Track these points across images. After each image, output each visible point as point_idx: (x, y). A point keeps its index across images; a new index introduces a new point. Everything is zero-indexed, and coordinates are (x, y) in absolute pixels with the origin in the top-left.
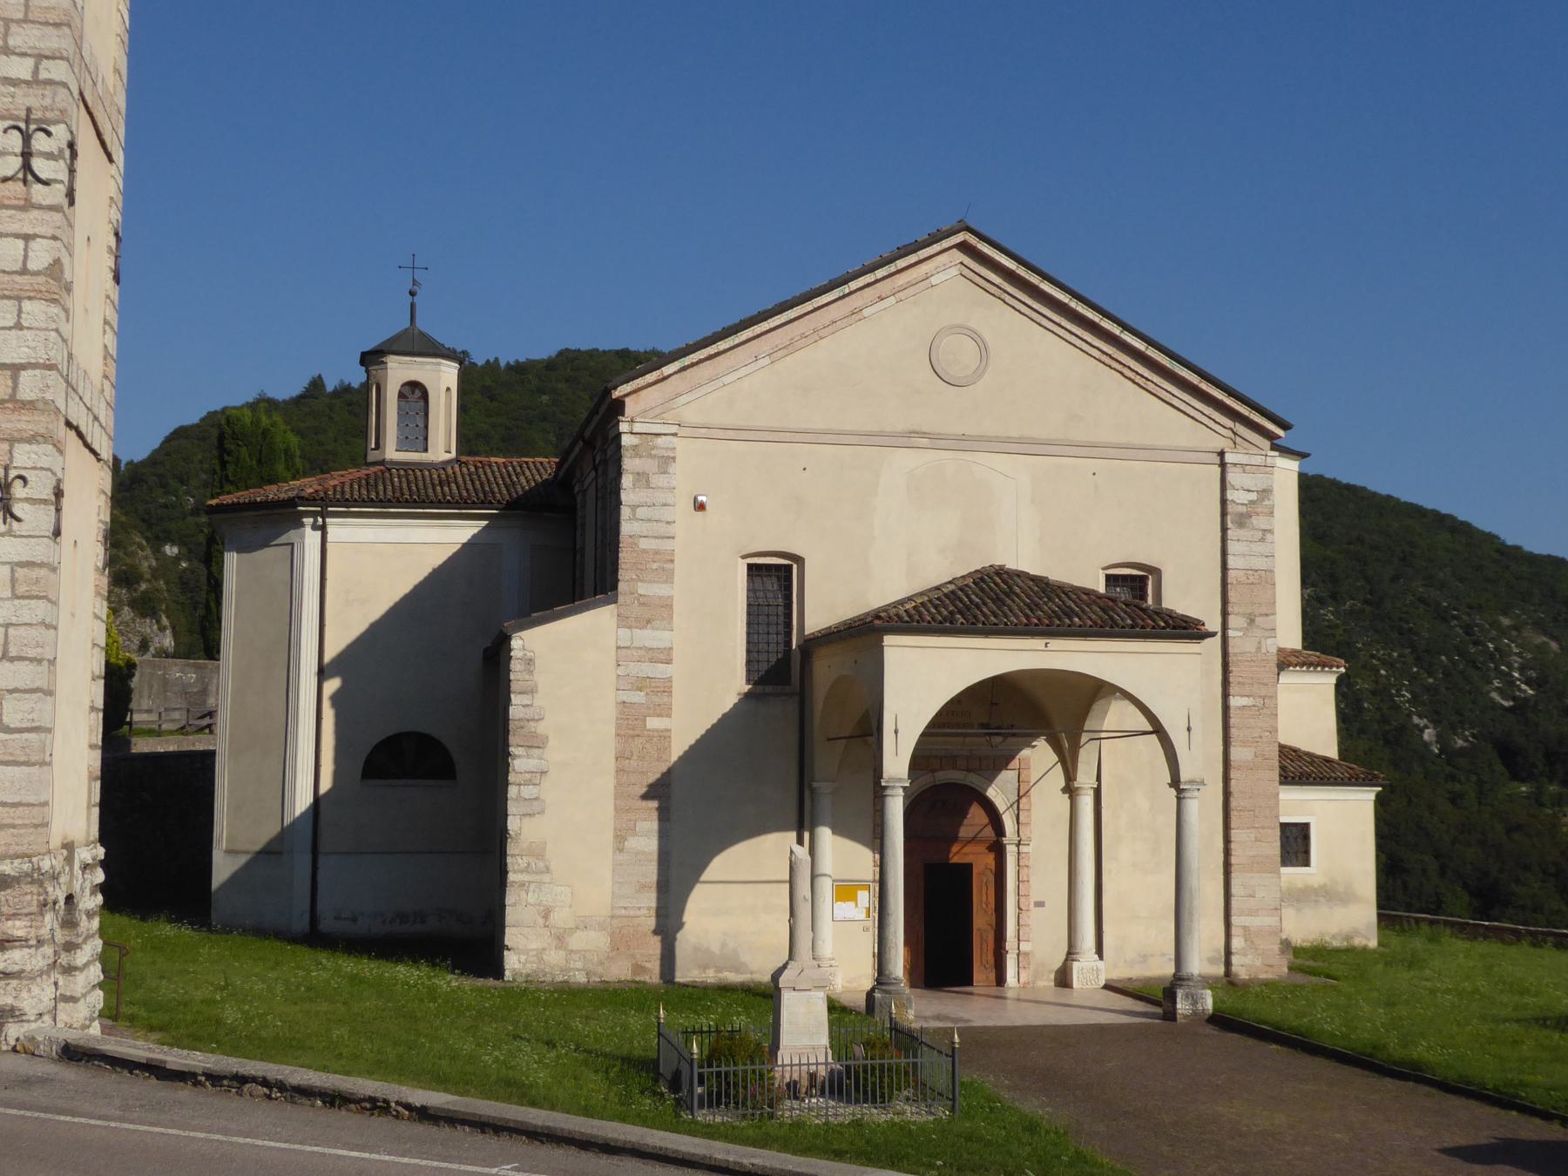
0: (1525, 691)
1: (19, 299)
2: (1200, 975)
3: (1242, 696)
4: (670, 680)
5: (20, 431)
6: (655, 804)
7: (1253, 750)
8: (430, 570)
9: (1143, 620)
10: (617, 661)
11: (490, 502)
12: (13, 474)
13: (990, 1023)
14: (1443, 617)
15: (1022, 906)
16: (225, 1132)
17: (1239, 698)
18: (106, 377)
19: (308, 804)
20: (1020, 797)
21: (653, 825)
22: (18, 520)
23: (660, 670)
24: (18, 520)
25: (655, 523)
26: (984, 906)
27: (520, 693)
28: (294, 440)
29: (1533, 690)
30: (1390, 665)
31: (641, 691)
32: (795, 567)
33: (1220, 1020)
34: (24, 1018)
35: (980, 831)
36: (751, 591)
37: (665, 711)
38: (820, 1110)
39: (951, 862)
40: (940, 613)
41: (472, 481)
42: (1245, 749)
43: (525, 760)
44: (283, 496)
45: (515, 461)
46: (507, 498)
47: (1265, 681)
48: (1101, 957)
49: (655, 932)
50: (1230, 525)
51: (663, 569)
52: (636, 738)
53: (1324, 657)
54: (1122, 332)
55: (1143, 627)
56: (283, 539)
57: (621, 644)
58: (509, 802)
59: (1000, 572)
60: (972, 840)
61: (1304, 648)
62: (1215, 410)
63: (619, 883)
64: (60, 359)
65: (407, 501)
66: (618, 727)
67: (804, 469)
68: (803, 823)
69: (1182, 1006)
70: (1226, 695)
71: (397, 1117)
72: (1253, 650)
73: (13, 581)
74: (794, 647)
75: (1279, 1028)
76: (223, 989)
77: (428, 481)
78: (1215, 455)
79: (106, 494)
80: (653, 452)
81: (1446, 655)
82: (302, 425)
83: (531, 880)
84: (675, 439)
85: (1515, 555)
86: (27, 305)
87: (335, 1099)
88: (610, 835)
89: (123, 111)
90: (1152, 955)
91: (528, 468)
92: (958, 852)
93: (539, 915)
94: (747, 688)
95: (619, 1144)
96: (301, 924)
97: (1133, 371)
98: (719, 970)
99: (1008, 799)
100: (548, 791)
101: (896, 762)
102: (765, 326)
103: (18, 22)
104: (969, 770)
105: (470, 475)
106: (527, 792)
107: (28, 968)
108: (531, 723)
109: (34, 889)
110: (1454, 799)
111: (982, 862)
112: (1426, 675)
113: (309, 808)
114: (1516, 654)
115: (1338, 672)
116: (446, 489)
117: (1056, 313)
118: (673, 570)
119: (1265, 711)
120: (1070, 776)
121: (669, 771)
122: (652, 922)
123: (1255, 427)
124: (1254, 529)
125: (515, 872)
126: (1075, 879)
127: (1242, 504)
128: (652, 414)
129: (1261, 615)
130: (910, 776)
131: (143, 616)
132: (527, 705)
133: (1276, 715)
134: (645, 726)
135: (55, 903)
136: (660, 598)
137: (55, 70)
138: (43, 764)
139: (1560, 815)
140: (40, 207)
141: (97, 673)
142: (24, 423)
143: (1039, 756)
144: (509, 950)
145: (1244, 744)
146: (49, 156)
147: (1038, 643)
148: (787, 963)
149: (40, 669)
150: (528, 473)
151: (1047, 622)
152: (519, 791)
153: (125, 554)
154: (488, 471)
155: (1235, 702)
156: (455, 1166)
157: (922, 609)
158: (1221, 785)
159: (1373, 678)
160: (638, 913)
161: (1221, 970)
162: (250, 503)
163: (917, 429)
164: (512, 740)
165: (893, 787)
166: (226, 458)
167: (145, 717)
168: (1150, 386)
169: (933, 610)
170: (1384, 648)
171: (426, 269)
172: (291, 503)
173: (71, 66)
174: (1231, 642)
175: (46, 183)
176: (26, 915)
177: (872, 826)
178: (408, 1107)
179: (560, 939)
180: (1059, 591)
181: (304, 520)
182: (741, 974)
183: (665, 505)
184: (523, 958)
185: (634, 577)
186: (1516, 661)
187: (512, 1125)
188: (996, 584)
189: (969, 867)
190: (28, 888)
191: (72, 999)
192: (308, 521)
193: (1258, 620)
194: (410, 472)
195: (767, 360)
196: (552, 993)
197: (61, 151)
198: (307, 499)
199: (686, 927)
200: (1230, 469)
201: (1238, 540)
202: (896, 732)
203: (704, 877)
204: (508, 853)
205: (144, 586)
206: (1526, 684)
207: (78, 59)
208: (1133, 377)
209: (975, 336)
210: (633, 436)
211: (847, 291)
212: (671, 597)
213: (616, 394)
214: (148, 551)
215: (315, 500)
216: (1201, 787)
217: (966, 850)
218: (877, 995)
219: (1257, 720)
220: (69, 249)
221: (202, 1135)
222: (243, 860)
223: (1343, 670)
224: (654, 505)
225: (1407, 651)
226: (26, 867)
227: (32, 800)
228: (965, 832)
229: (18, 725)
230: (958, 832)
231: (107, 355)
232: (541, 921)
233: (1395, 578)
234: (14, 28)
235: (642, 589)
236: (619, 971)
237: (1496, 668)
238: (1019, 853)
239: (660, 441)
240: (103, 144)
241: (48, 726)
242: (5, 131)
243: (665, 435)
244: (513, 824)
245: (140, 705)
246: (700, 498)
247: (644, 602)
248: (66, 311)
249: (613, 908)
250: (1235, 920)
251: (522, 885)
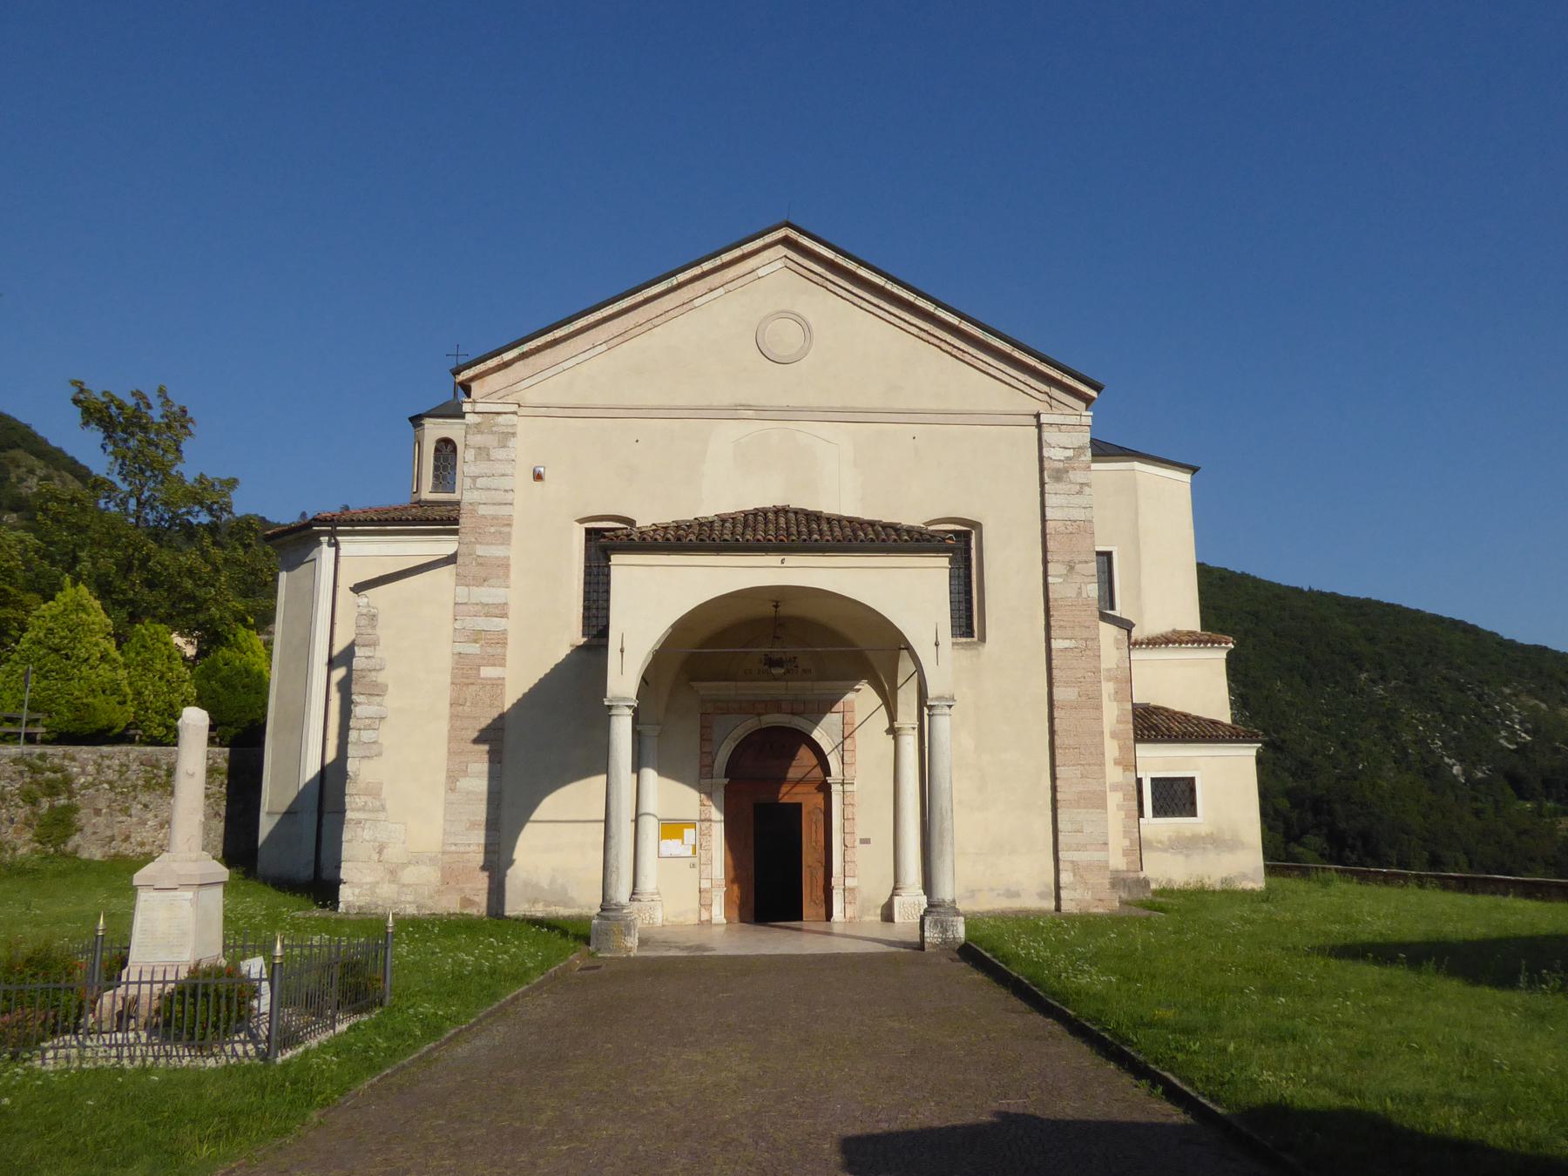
0: (1524, 738)
3: (1063, 639)
4: (505, 632)
7: (1076, 690)
10: (455, 616)
14: (1461, 689)
15: (847, 844)
17: (1061, 640)
19: (316, 772)
23: (496, 624)
25: (493, 492)
26: (814, 844)
27: (363, 646)
29: (1530, 736)
30: (1426, 723)
31: (476, 643)
35: (809, 772)
37: (500, 661)
39: (781, 801)
42: (1069, 689)
47: (1086, 624)
49: (483, 868)
52: (470, 686)
53: (1214, 636)
54: (936, 309)
56: (310, 557)
57: (458, 600)
58: (349, 746)
60: (798, 782)
62: (1031, 377)
63: (451, 821)
66: (454, 676)
67: (637, 441)
78: (1032, 417)
80: (494, 429)
81: (1465, 715)
83: (366, 817)
84: (514, 417)
85: (1511, 645)
88: (442, 776)
90: (980, 890)
92: (787, 793)
93: (374, 850)
94: (581, 641)
97: (949, 344)
98: (547, 904)
99: (833, 741)
100: (386, 735)
104: (793, 714)
108: (374, 673)
110: (1477, 813)
111: (810, 801)
112: (1451, 729)
114: (1516, 713)
115: (1225, 648)
117: (874, 296)
118: (509, 534)
119: (1088, 652)
120: (892, 717)
122: (480, 859)
123: (1057, 385)
124: (1071, 482)
125: (353, 810)
127: (1060, 461)
129: (1080, 562)
132: (370, 657)
133: (1099, 656)
134: (479, 675)
136: (497, 558)
139: (1557, 823)
144: (345, 883)
145: (1067, 684)
147: (773, 560)
152: (359, 735)
155: (1055, 644)
158: (1047, 724)
159: (1414, 732)
160: (468, 849)
161: (1052, 905)
163: (744, 402)
165: (618, 707)
168: (967, 358)
170: (1420, 712)
171: (458, 346)
174: (1051, 588)
177: (698, 767)
181: (321, 538)
182: (569, 908)
183: (503, 475)
184: (357, 891)
185: (473, 540)
186: (1517, 718)
189: (798, 807)
192: (324, 539)
193: (1078, 567)
198: (320, 520)
199: (516, 863)
200: (1045, 428)
201: (1056, 494)
202: (622, 651)
203: (534, 817)
204: (347, 792)
206: (1525, 733)
208: (950, 350)
209: (799, 320)
210: (476, 415)
217: (795, 790)
219: (1080, 661)
222: (277, 818)
223: (1231, 646)
224: (493, 475)
225: (1437, 714)
228: (793, 773)
230: (787, 772)
232: (376, 857)
233: (1426, 664)
236: (449, 904)
237: (1503, 723)
239: (501, 419)
243: (505, 413)
247: (482, 562)
251: (359, 822)
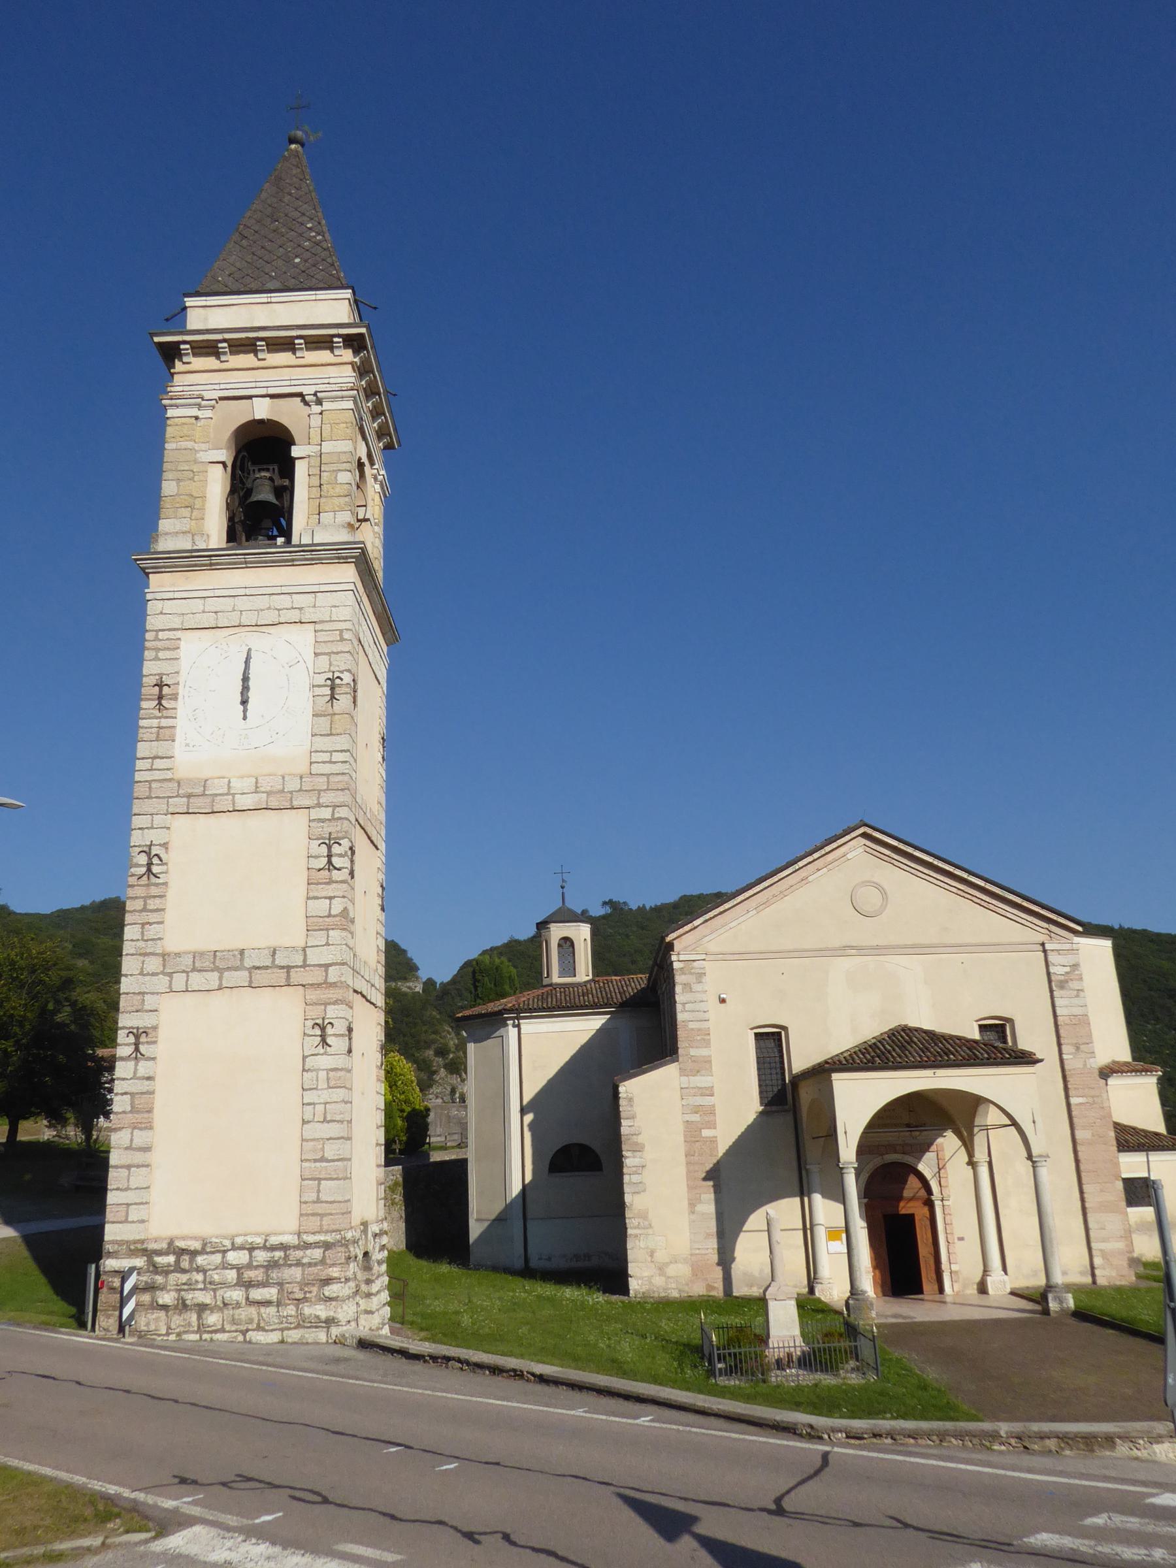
1: (327, 930)
2: (1063, 1284)
3: (1078, 1097)
4: (714, 1106)
5: (329, 998)
6: (711, 1183)
8: (579, 1046)
9: (995, 1054)
11: (611, 1004)
12: (326, 1021)
13: (927, 1319)
16: (433, 1390)
18: (379, 962)
20: (940, 1169)
21: (711, 1196)
22: (330, 1046)
23: (707, 1101)
24: (330, 1046)
28: (514, 971)
32: (783, 1033)
33: (1080, 1315)
34: (340, 1323)
36: (758, 1049)
37: (712, 1125)
38: (795, 1376)
40: (865, 1057)
41: (601, 992)
43: (631, 1159)
44: (496, 1009)
45: (626, 978)
46: (620, 1000)
47: (1093, 1086)
48: (1006, 1273)
49: (718, 1264)
50: (1054, 988)
51: (704, 1040)
53: (1146, 1066)
55: (995, 1059)
56: (497, 1034)
57: (683, 1086)
59: (905, 1029)
61: (1134, 1059)
64: (348, 959)
65: (563, 1007)
66: (685, 1136)
68: (803, 1191)
69: (1053, 1305)
70: (1067, 1097)
71: (527, 1381)
72: (1082, 1067)
73: (328, 1079)
74: (787, 1082)
75: (1114, 1319)
76: (465, 1304)
77: (576, 993)
79: (381, 1025)
80: (693, 971)
82: (535, 953)
86: (331, 932)
87: (496, 1370)
88: (686, 1203)
89: (384, 822)
91: (634, 982)
94: (761, 1108)
95: (645, 1397)
96: (519, 1264)
101: (848, 1152)
102: (751, 892)
103: (324, 790)
105: (600, 988)
106: (635, 1178)
107: (341, 1295)
108: (634, 1137)
109: (343, 1249)
111: (921, 1212)
113: (519, 1194)
116: (586, 998)
118: (710, 1040)
121: (718, 1162)
122: (715, 1258)
125: (631, 1228)
126: (984, 1221)
128: (690, 949)
129: (1083, 1044)
130: (857, 1161)
131: (452, 1073)
135: (356, 1257)
136: (704, 1057)
137: (342, 812)
138: (345, 1178)
140: (337, 882)
141: (379, 1124)
142: (332, 994)
143: (949, 1142)
146: (340, 855)
147: (928, 1072)
148: (770, 1283)
149: (342, 1126)
150: (633, 984)
151: (933, 1059)
153: (441, 1037)
154: (611, 985)
155: (1073, 1101)
156: (551, 1410)
157: (854, 1056)
161: (1089, 1280)
162: (478, 1014)
163: (848, 944)
164: (624, 1147)
165: (847, 1168)
166: (477, 984)
167: (439, 1139)
168: (992, 907)
169: (861, 1056)
172: (500, 1013)
173: (350, 809)
174: (1066, 1062)
175: (339, 869)
176: (340, 1264)
178: (533, 1374)
179: (661, 1269)
180: (942, 1039)
184: (640, 1282)
187: (587, 1385)
188: (902, 1037)
189: (913, 1215)
190: (340, 1249)
191: (371, 1312)
192: (510, 1022)
194: (567, 989)
195: (755, 912)
196: (652, 1304)
197: (346, 852)
199: (737, 1260)
200: (1049, 953)
202: (846, 1133)
203: (744, 1229)
205: (451, 1056)
207: (355, 804)
211: (797, 868)
212: (710, 1056)
213: (668, 939)
214: (453, 1035)
215: (513, 1010)
216: (1048, 1159)
218: (851, 1302)
220: (352, 902)
221: (420, 1391)
226: (338, 1237)
227: (340, 1199)
228: (907, 1193)
229: (332, 1158)
231: (379, 950)
232: (649, 1259)
234: (322, 794)
235: (693, 1052)
236: (698, 1290)
238: (943, 1206)
239: (696, 964)
240: (372, 842)
241: (349, 1157)
242: (319, 845)
244: (628, 1198)
245: (435, 1131)
246: (722, 996)
247: (694, 1060)
248: (352, 933)
249: (691, 1249)
250: (1093, 1245)
251: (636, 1236)
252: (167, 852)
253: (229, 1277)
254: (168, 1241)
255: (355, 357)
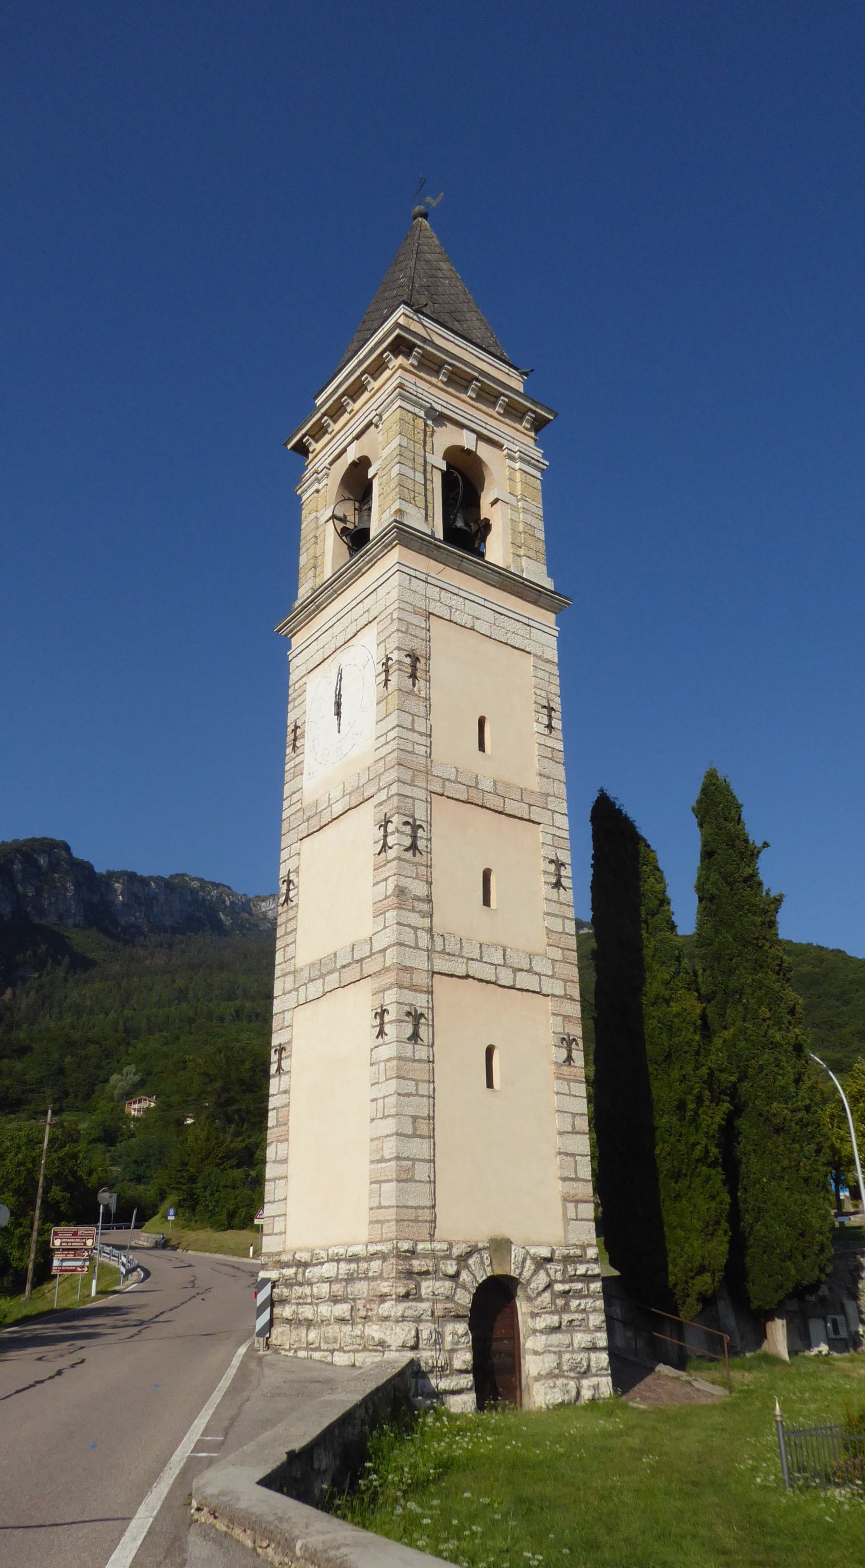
252: (298, 877)
253: (324, 1291)
254: (292, 1253)
255: (408, 360)
